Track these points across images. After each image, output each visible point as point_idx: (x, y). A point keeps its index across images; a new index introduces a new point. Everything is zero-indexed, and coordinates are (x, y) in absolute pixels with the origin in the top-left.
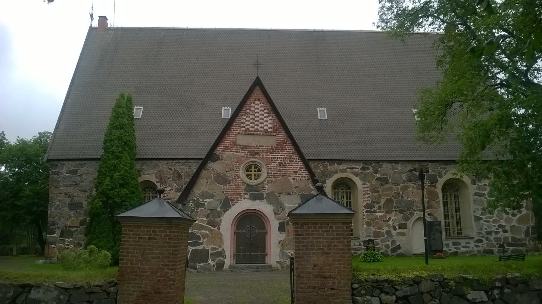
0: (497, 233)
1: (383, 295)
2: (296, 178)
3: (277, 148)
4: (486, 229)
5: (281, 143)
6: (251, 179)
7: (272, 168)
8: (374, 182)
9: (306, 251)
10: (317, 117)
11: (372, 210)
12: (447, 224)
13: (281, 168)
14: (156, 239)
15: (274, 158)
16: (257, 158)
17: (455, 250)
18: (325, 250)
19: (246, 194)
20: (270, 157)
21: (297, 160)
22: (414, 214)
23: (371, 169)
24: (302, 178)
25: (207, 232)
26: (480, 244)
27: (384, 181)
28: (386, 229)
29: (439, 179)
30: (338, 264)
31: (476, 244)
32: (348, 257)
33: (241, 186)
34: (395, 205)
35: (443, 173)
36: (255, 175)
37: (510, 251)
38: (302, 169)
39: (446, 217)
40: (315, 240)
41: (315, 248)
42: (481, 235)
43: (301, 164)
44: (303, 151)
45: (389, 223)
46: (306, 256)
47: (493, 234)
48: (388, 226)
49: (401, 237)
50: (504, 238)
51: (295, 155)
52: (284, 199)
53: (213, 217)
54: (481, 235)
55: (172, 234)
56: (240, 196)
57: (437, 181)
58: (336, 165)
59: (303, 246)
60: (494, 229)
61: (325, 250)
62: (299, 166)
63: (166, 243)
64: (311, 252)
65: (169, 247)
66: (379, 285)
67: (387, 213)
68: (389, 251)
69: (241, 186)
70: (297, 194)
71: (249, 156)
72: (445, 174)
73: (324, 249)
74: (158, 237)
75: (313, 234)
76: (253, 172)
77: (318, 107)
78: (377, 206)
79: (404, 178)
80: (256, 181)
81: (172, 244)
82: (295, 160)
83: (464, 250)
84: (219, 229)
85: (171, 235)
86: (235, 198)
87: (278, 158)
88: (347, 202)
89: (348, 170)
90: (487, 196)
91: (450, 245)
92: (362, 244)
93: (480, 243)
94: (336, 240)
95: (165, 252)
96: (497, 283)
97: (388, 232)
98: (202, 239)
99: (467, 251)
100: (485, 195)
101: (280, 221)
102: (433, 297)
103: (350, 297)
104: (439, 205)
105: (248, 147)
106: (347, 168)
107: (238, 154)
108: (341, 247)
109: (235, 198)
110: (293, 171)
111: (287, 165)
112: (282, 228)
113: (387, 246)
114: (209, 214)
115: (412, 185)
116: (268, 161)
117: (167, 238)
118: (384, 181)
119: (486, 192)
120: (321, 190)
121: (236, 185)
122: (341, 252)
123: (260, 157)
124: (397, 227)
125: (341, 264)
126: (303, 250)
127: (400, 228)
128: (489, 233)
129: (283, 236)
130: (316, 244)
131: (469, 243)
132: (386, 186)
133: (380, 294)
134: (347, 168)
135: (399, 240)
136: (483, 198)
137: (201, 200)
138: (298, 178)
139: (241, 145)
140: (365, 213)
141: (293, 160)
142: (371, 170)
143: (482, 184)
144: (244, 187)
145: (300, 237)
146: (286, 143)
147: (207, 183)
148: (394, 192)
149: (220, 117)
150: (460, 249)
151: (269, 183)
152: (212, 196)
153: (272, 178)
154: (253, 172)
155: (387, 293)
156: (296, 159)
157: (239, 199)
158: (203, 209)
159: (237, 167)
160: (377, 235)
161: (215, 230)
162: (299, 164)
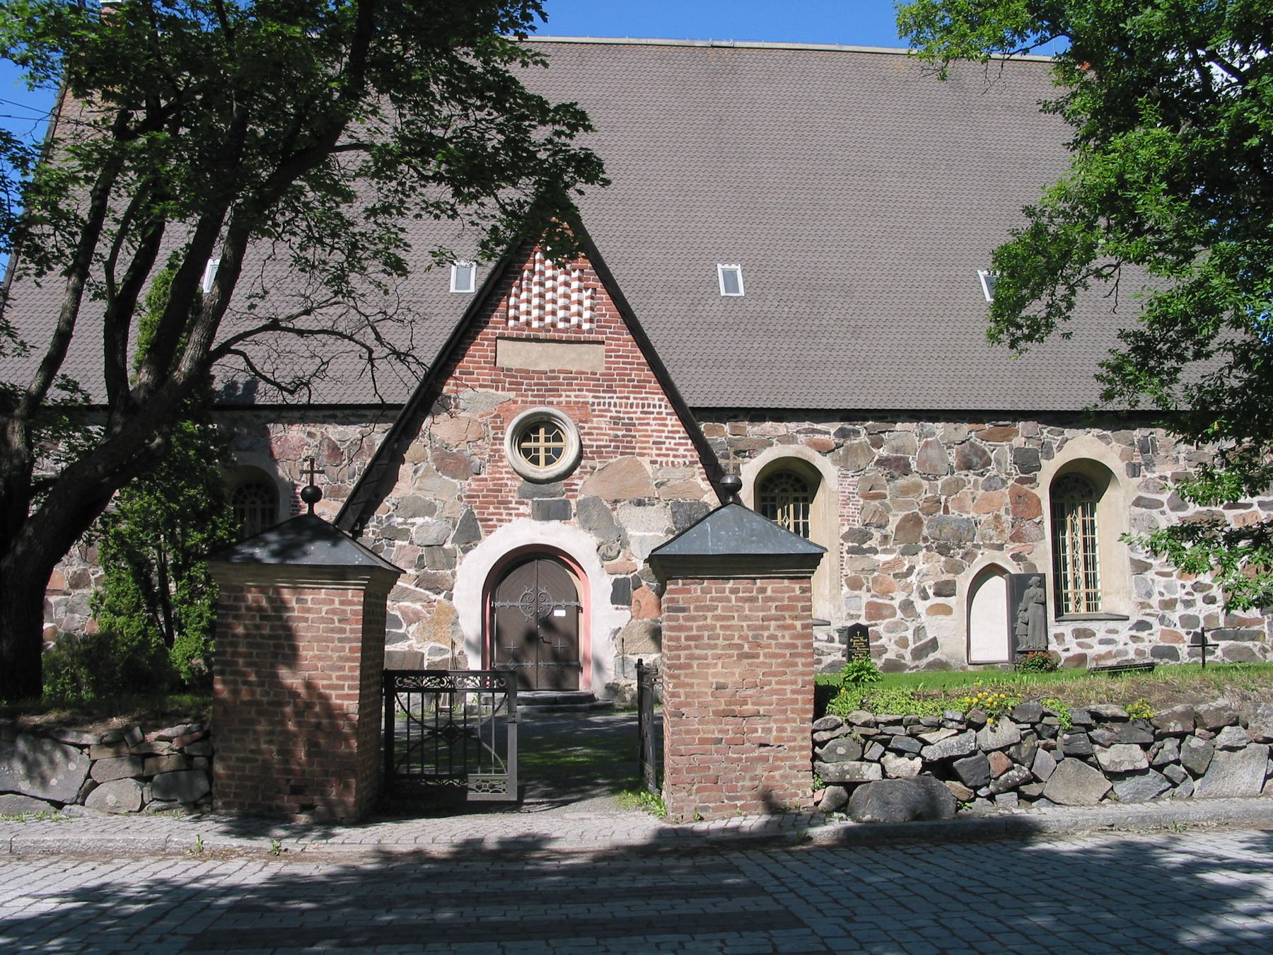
0: (1188, 604)
1: (890, 756)
2: (659, 459)
3: (608, 376)
4: (1161, 594)
5: (618, 363)
6: (535, 461)
7: (595, 432)
8: (872, 471)
9: (697, 652)
10: (716, 290)
11: (865, 546)
12: (1059, 582)
13: (620, 433)
14: (306, 620)
15: (599, 404)
16: (552, 403)
17: (1079, 651)
18: (746, 648)
19: (522, 503)
20: (587, 403)
21: (663, 409)
22: (976, 556)
23: (863, 432)
24: (676, 460)
25: (418, 606)
26: (1144, 634)
27: (898, 466)
28: (899, 597)
29: (1043, 462)
30: (778, 683)
31: (1134, 633)
32: (804, 665)
33: (509, 482)
34: (925, 532)
35: (1055, 446)
36: (547, 450)
37: (1219, 652)
38: (677, 436)
39: (1058, 564)
40: (718, 624)
41: (721, 642)
42: (1148, 611)
43: (674, 422)
44: (683, 391)
45: (909, 580)
46: (695, 663)
47: (1179, 606)
48: (907, 587)
49: (940, 617)
50: (1205, 618)
51: (656, 397)
52: (627, 516)
53: (433, 564)
54: (1148, 611)
55: (349, 608)
56: (505, 509)
57: (1039, 468)
58: (768, 425)
59: (687, 638)
60: (1180, 594)
61: (746, 648)
62: (666, 425)
63: (332, 630)
64: (710, 652)
65: (341, 640)
66: (882, 733)
67: (903, 554)
68: (908, 657)
69: (509, 482)
70: (663, 504)
71: (530, 399)
72: (1060, 448)
73: (742, 646)
74: (311, 616)
75: (716, 608)
76: (542, 444)
77: (745, 298)
78: (877, 534)
79: (953, 459)
80: (550, 467)
81: (348, 634)
82: (657, 410)
83: (1103, 649)
84: (450, 598)
85: (344, 611)
86: (493, 514)
87: (610, 404)
88: (796, 525)
89: (801, 437)
90: (1166, 508)
91: (1066, 638)
92: (836, 636)
93: (1143, 630)
94: (773, 623)
95: (330, 653)
96: (1172, 724)
97: (907, 606)
98: (405, 625)
99: (1110, 652)
100: (1162, 504)
101: (614, 577)
102: (1015, 761)
103: (808, 762)
104: (1043, 533)
105: (527, 374)
106: (798, 432)
107: (500, 392)
108: (787, 640)
109: (493, 514)
110: (651, 440)
111: (634, 425)
112: (621, 594)
113: (903, 643)
114: (421, 557)
115: (972, 478)
116: (583, 414)
117: (336, 618)
118: (898, 466)
119: (1164, 497)
120: (728, 493)
121: (494, 479)
122: (787, 652)
123: (559, 403)
124: (930, 592)
125: (785, 683)
126: (688, 647)
127: (937, 594)
128: (1169, 605)
129: (622, 616)
130: (721, 633)
131: (1115, 632)
132: (902, 481)
133: (883, 755)
134: (798, 432)
135: (935, 627)
136: (1155, 512)
137: (400, 520)
138: (664, 459)
139: (508, 370)
140: (845, 555)
141: (651, 409)
142: (863, 438)
143: (1156, 475)
144: (518, 484)
145: (681, 615)
146: (632, 363)
147: (416, 472)
148: (923, 496)
149: (445, 288)
150: (1091, 647)
151: (586, 473)
152: (430, 510)
153: (593, 459)
154: (542, 444)
155: (900, 753)
156: (660, 406)
157: (504, 517)
158: (406, 543)
159: (499, 428)
160: (876, 611)
161: (439, 602)
162: (668, 422)
